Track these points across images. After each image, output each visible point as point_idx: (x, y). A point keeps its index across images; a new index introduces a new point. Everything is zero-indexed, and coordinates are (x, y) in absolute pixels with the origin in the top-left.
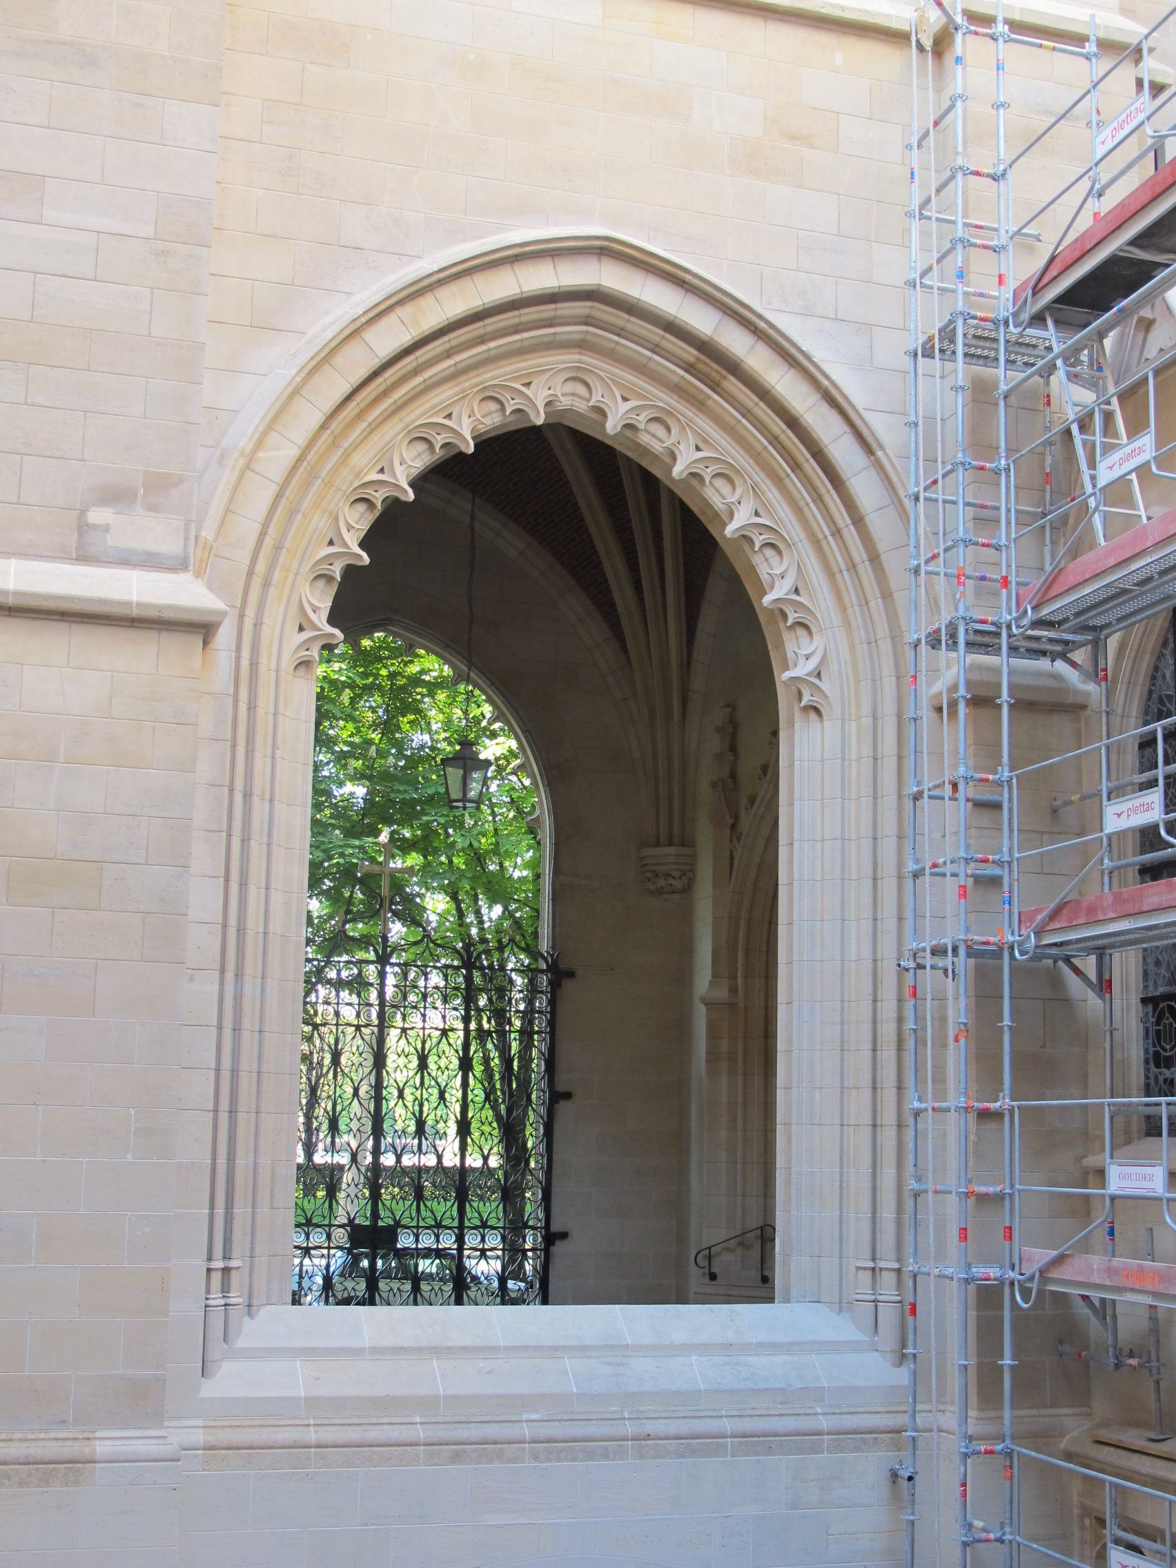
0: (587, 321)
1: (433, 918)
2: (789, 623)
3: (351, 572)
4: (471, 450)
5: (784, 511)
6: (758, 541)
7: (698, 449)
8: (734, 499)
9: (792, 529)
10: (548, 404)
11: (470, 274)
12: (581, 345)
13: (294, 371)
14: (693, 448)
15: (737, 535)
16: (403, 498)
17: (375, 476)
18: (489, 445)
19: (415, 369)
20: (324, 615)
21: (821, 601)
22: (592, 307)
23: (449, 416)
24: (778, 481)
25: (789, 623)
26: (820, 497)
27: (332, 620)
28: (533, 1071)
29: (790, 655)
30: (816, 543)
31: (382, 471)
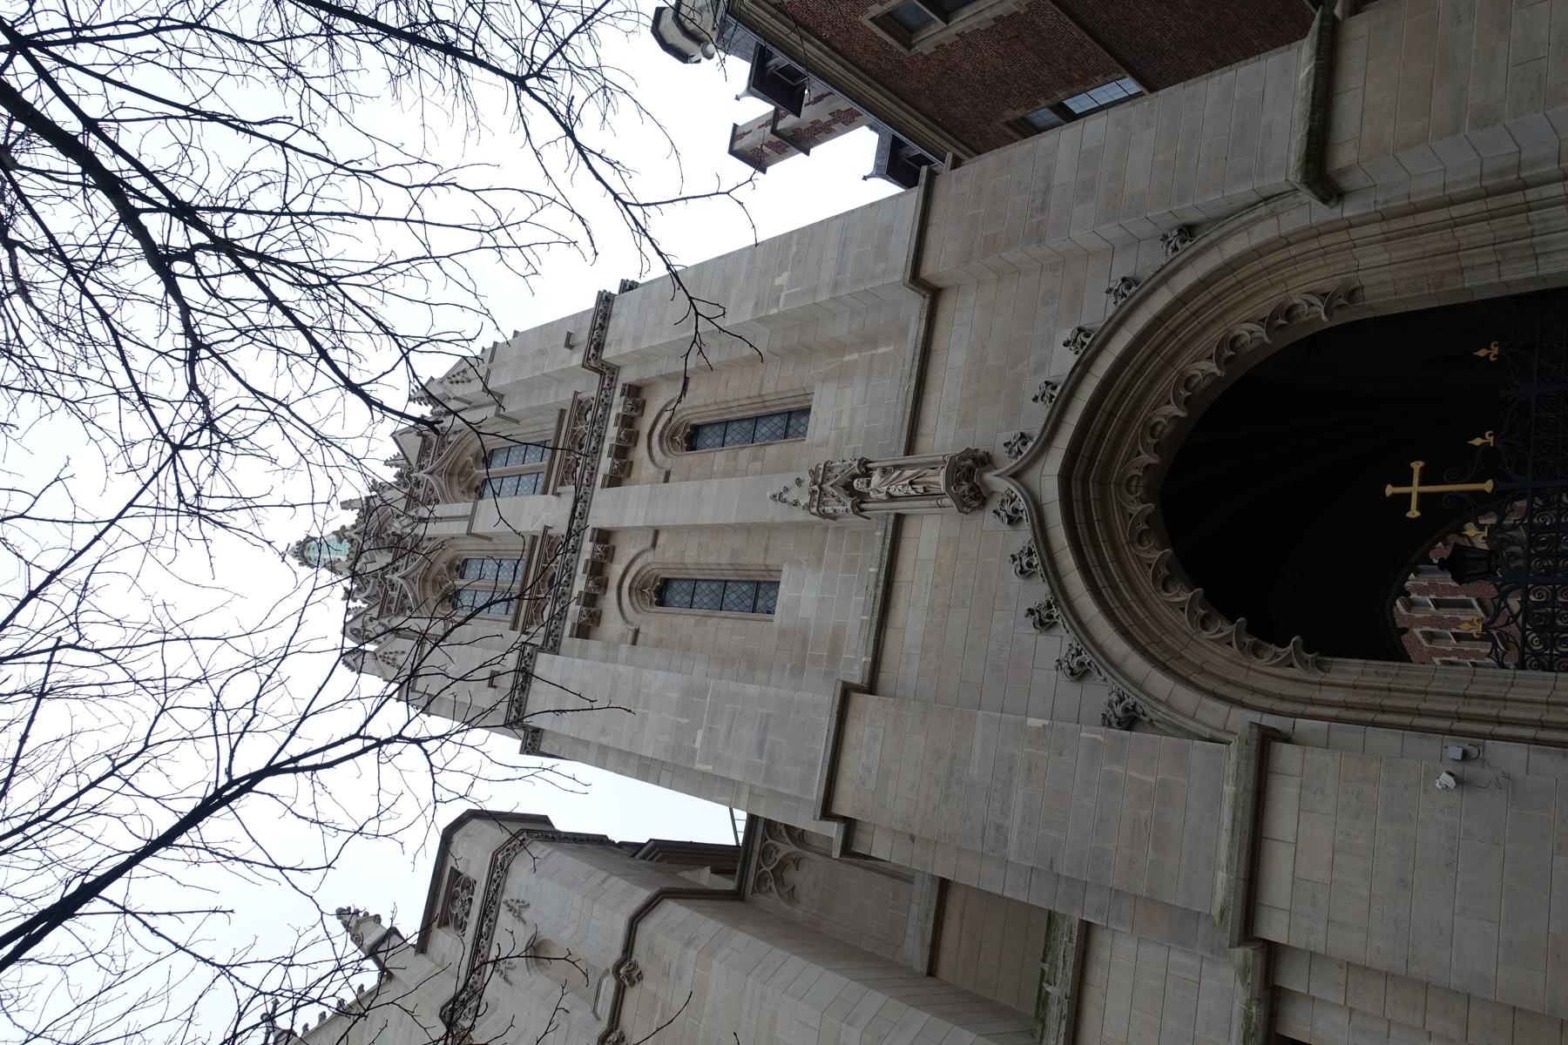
0: (1085, 481)
1: (429, 415)
2: (1232, 353)
3: (1251, 630)
4: (1200, 589)
5: (1159, 389)
6: (1185, 394)
7: (1139, 454)
8: (1200, 374)
9: (1171, 376)
10: (1143, 503)
11: (1071, 602)
12: (1103, 483)
13: (902, 275)
14: (1169, 406)
15: (1185, 409)
16: (1245, 625)
17: (1235, 649)
18: (1193, 578)
19: (1112, 588)
20: (1280, 650)
21: (1264, 305)
22: (1076, 479)
23: (1131, 515)
24: (1139, 402)
25: (1232, 353)
26: (1099, 436)
27: (1284, 645)
28: (1502, 517)
29: (1255, 344)
30: (1170, 362)
31: (1183, 610)
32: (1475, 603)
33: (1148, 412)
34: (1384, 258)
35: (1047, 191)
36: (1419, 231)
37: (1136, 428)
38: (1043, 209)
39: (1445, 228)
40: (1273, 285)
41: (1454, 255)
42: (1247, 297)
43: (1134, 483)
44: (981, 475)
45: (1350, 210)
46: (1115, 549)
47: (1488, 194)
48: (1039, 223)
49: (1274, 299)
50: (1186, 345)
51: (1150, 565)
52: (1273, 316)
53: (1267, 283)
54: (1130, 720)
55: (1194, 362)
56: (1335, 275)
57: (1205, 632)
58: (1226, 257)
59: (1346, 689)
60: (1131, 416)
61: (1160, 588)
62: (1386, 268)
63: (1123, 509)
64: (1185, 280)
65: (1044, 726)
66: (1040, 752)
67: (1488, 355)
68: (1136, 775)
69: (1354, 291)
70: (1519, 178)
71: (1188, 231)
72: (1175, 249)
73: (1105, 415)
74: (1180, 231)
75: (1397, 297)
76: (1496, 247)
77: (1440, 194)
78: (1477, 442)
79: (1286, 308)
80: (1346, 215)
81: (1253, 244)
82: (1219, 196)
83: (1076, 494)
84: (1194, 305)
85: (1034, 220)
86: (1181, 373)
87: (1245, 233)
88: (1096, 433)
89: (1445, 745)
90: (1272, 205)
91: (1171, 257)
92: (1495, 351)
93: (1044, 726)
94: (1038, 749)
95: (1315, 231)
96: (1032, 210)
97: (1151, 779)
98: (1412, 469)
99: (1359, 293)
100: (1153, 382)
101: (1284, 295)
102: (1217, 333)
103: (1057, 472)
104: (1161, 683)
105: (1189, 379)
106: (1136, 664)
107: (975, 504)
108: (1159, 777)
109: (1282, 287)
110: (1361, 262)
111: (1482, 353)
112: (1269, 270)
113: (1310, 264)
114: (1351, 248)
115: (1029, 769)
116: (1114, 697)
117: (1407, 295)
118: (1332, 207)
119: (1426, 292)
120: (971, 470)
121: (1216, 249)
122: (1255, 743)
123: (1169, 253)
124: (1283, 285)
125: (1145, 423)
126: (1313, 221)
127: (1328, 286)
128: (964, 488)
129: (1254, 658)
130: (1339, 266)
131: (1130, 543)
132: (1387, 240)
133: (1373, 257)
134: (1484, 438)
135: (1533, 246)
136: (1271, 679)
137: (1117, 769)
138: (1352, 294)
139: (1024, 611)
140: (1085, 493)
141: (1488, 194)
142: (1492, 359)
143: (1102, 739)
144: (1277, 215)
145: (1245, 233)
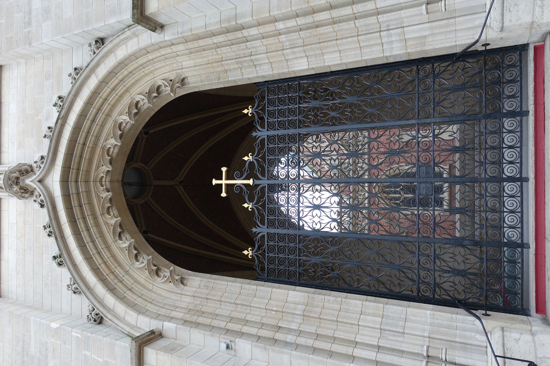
12: (87, 181)
15: (119, 141)
21: (145, 86)
24: (98, 137)
30: (108, 115)
32: (326, 141)
33: (103, 142)
34: (192, 63)
35: (30, 13)
36: (204, 49)
37: (98, 150)
38: (29, 23)
39: (213, 49)
40: (146, 75)
41: (220, 63)
42: (137, 81)
43: (104, 180)
44: (24, 181)
45: (167, 36)
46: (95, 218)
47: (228, 31)
48: (29, 32)
49: (149, 82)
50: (114, 106)
51: (112, 225)
52: (150, 93)
53: (143, 74)
54: (99, 320)
55: (120, 115)
56: (173, 70)
57: (137, 263)
58: (118, 59)
59: (191, 297)
60: (96, 144)
61: (117, 238)
62: (193, 68)
63: (98, 196)
64: (102, 71)
65: (57, 327)
66: (57, 342)
67: (248, 113)
68: (96, 357)
69: (183, 80)
70: (237, 24)
71: (101, 41)
72: (94, 53)
73: (80, 145)
74: (97, 42)
75: (202, 83)
76: (237, 60)
77: (204, 30)
78: (246, 158)
79: (156, 87)
80: (166, 39)
81: (129, 52)
82: (103, 24)
83: (72, 190)
84: (112, 85)
85: (26, 30)
86: (115, 121)
87: (125, 45)
88: (78, 155)
89: (220, 341)
90: (132, 30)
91: (93, 57)
92: (250, 111)
93: (57, 327)
94: (56, 340)
95: (157, 47)
96: (25, 23)
97: (101, 360)
98: (222, 171)
99: (186, 81)
100: (103, 126)
101: (153, 80)
102: (126, 101)
103: (59, 180)
104: (110, 300)
105: (121, 124)
106: (100, 289)
107: (27, 195)
108: (104, 359)
109: (152, 76)
110: (184, 64)
111: (246, 111)
112: (143, 66)
113: (159, 65)
114: (175, 57)
115: (54, 350)
116: (91, 309)
117: (206, 83)
118: (160, 34)
119: (214, 82)
120: (17, 178)
121: (113, 54)
122: (134, 351)
123: (92, 55)
124: (152, 74)
125: (103, 148)
126: (152, 41)
127: (172, 78)
128: (15, 189)
129: (156, 277)
130: (175, 65)
131: (103, 214)
132: (191, 53)
133: (187, 62)
134: (249, 157)
135: (252, 61)
136: (162, 290)
137: (88, 353)
138: (183, 81)
139: (51, 258)
140: (77, 188)
141: (228, 31)
142: (250, 115)
143: (80, 337)
144: (137, 36)
145: (125, 45)
